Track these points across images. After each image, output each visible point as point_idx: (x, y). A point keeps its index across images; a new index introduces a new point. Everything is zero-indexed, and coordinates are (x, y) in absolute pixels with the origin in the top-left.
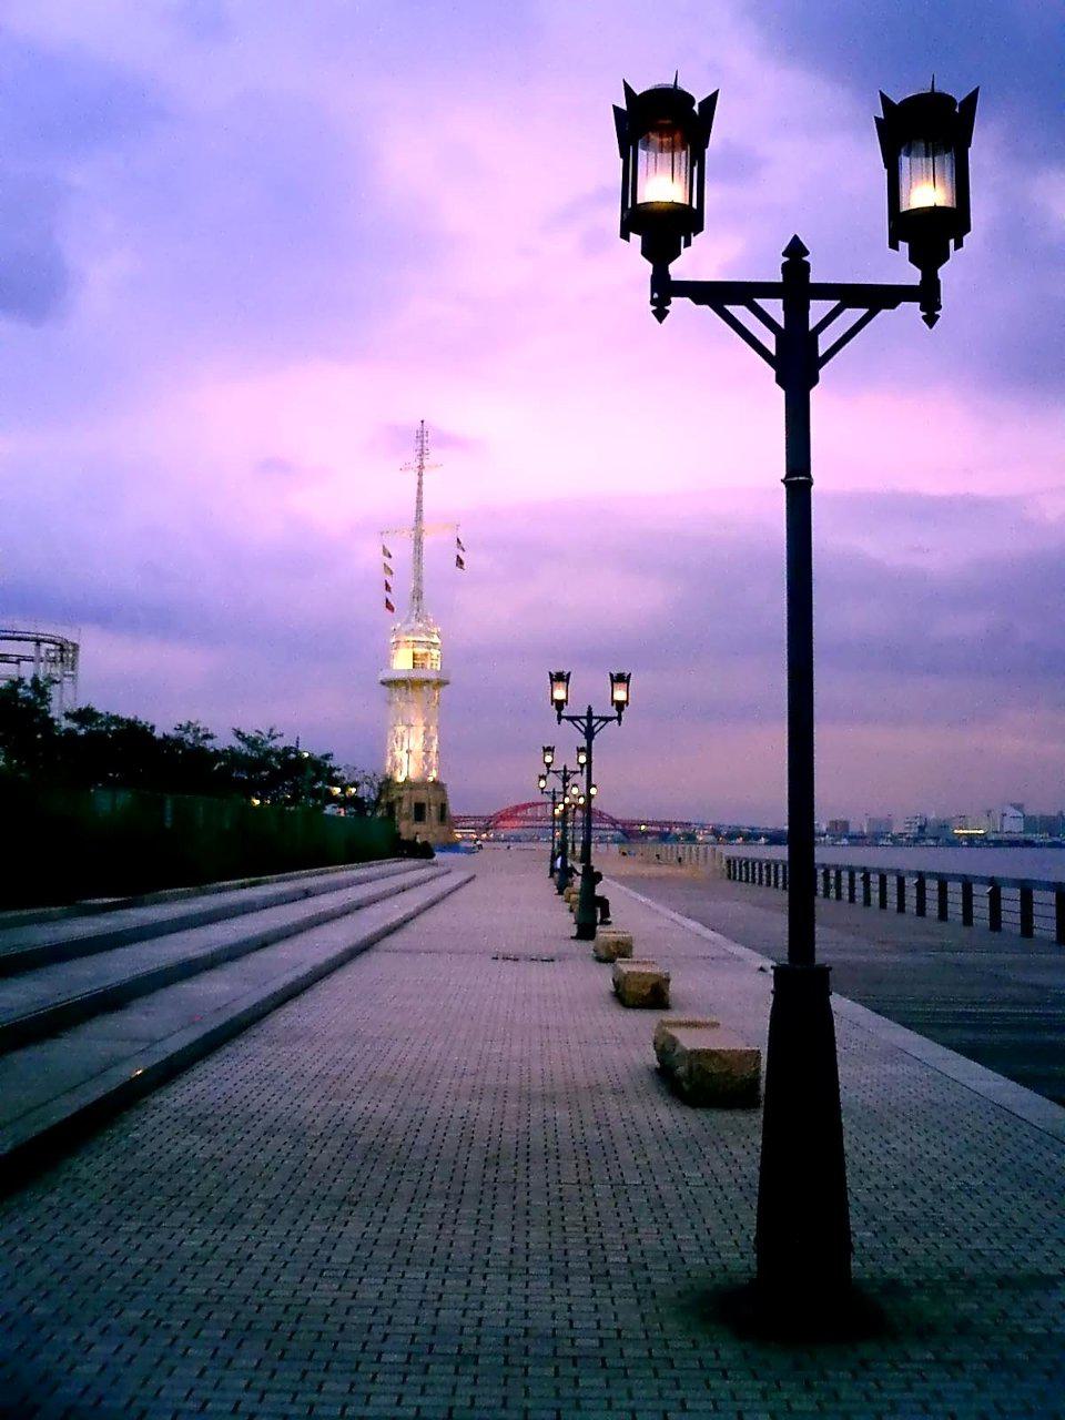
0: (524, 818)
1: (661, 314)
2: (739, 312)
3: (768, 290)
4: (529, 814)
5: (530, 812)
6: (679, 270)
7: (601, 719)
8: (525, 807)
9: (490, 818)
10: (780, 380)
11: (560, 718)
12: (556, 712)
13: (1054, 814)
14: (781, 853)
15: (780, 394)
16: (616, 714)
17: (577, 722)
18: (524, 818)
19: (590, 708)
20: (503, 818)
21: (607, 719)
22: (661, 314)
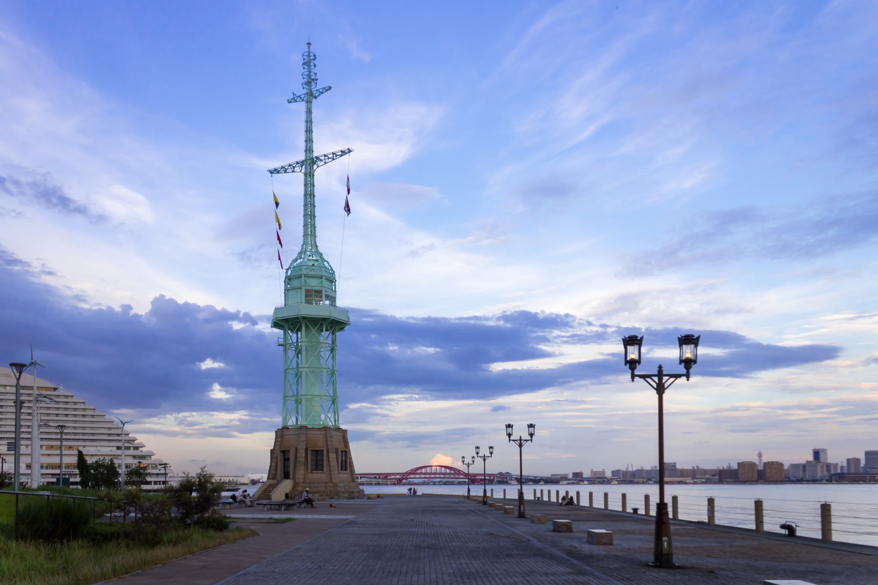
0: (419, 474)
1: (633, 381)
2: (649, 380)
3: (654, 375)
4: (423, 472)
5: (423, 470)
6: (636, 373)
7: (525, 440)
8: (421, 468)
9: (403, 474)
10: (657, 393)
11: (510, 440)
12: (508, 438)
13: (691, 468)
14: (666, 479)
15: (657, 396)
16: (530, 439)
17: (516, 442)
18: (419, 474)
19: (521, 437)
20: (410, 474)
21: (527, 440)
22: (633, 381)
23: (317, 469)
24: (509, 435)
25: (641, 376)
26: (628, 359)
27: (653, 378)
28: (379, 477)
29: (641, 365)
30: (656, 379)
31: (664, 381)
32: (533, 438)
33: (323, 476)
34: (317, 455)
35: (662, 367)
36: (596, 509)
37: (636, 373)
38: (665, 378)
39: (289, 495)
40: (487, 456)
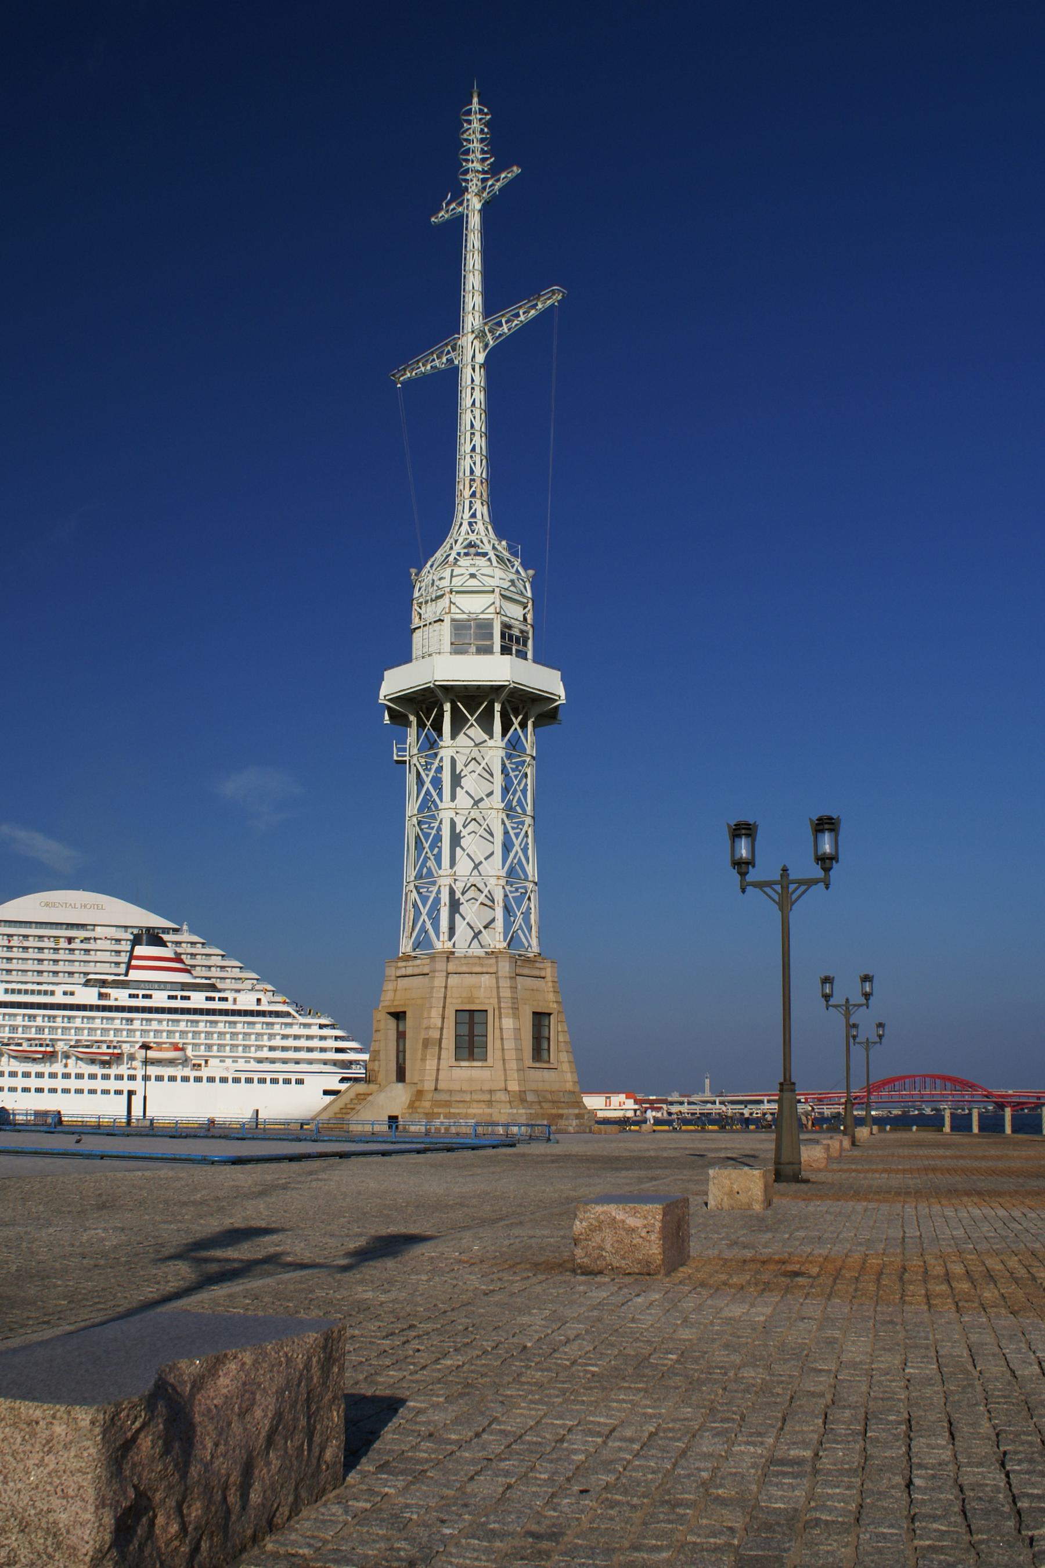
3: (776, 883)
7: (855, 1005)
16: (865, 1001)
23: (471, 1057)
24: (827, 997)
25: (756, 885)
26: (820, 853)
27: (775, 887)
28: (806, 1099)
29: (839, 864)
30: (778, 888)
31: (791, 890)
32: (870, 1001)
33: (485, 1074)
34: (472, 1024)
35: (787, 870)
36: (91, 1144)
37: (749, 878)
38: (792, 887)
39: (400, 1119)
40: (874, 1041)
